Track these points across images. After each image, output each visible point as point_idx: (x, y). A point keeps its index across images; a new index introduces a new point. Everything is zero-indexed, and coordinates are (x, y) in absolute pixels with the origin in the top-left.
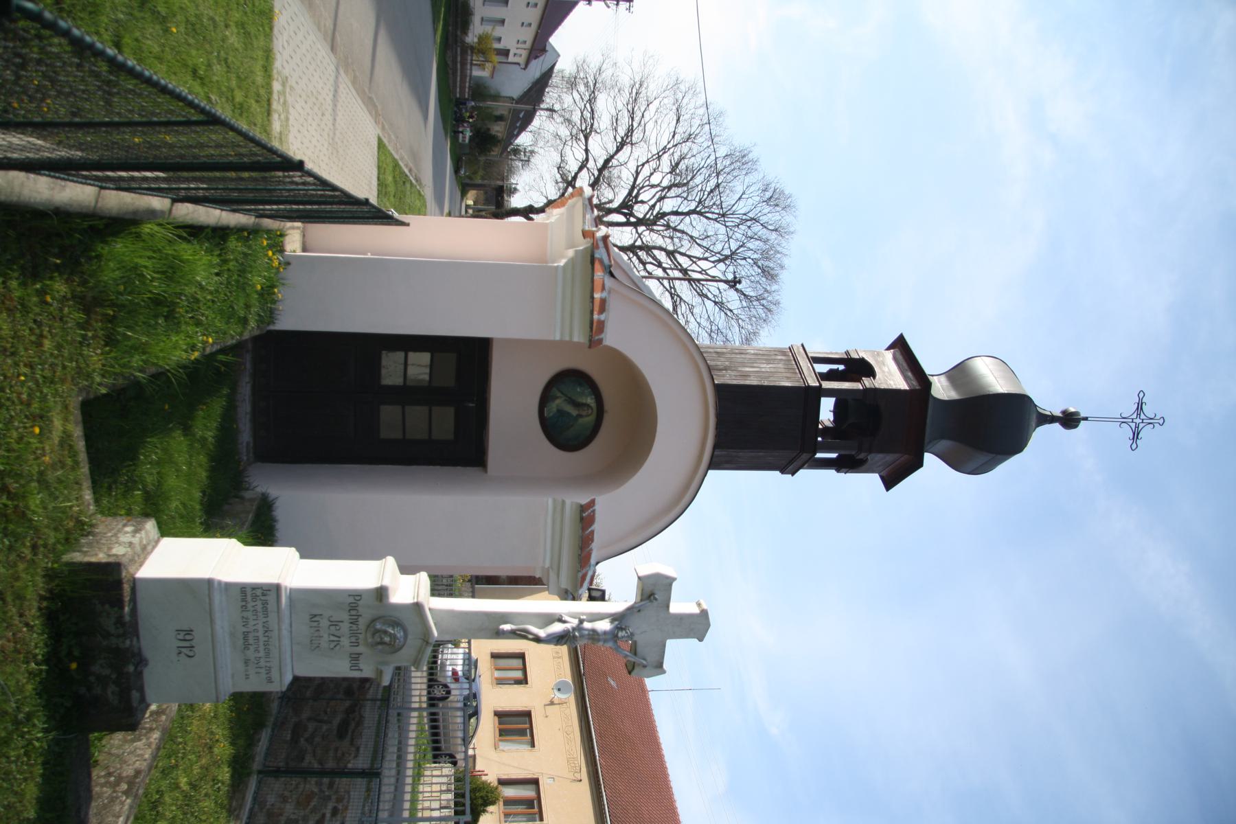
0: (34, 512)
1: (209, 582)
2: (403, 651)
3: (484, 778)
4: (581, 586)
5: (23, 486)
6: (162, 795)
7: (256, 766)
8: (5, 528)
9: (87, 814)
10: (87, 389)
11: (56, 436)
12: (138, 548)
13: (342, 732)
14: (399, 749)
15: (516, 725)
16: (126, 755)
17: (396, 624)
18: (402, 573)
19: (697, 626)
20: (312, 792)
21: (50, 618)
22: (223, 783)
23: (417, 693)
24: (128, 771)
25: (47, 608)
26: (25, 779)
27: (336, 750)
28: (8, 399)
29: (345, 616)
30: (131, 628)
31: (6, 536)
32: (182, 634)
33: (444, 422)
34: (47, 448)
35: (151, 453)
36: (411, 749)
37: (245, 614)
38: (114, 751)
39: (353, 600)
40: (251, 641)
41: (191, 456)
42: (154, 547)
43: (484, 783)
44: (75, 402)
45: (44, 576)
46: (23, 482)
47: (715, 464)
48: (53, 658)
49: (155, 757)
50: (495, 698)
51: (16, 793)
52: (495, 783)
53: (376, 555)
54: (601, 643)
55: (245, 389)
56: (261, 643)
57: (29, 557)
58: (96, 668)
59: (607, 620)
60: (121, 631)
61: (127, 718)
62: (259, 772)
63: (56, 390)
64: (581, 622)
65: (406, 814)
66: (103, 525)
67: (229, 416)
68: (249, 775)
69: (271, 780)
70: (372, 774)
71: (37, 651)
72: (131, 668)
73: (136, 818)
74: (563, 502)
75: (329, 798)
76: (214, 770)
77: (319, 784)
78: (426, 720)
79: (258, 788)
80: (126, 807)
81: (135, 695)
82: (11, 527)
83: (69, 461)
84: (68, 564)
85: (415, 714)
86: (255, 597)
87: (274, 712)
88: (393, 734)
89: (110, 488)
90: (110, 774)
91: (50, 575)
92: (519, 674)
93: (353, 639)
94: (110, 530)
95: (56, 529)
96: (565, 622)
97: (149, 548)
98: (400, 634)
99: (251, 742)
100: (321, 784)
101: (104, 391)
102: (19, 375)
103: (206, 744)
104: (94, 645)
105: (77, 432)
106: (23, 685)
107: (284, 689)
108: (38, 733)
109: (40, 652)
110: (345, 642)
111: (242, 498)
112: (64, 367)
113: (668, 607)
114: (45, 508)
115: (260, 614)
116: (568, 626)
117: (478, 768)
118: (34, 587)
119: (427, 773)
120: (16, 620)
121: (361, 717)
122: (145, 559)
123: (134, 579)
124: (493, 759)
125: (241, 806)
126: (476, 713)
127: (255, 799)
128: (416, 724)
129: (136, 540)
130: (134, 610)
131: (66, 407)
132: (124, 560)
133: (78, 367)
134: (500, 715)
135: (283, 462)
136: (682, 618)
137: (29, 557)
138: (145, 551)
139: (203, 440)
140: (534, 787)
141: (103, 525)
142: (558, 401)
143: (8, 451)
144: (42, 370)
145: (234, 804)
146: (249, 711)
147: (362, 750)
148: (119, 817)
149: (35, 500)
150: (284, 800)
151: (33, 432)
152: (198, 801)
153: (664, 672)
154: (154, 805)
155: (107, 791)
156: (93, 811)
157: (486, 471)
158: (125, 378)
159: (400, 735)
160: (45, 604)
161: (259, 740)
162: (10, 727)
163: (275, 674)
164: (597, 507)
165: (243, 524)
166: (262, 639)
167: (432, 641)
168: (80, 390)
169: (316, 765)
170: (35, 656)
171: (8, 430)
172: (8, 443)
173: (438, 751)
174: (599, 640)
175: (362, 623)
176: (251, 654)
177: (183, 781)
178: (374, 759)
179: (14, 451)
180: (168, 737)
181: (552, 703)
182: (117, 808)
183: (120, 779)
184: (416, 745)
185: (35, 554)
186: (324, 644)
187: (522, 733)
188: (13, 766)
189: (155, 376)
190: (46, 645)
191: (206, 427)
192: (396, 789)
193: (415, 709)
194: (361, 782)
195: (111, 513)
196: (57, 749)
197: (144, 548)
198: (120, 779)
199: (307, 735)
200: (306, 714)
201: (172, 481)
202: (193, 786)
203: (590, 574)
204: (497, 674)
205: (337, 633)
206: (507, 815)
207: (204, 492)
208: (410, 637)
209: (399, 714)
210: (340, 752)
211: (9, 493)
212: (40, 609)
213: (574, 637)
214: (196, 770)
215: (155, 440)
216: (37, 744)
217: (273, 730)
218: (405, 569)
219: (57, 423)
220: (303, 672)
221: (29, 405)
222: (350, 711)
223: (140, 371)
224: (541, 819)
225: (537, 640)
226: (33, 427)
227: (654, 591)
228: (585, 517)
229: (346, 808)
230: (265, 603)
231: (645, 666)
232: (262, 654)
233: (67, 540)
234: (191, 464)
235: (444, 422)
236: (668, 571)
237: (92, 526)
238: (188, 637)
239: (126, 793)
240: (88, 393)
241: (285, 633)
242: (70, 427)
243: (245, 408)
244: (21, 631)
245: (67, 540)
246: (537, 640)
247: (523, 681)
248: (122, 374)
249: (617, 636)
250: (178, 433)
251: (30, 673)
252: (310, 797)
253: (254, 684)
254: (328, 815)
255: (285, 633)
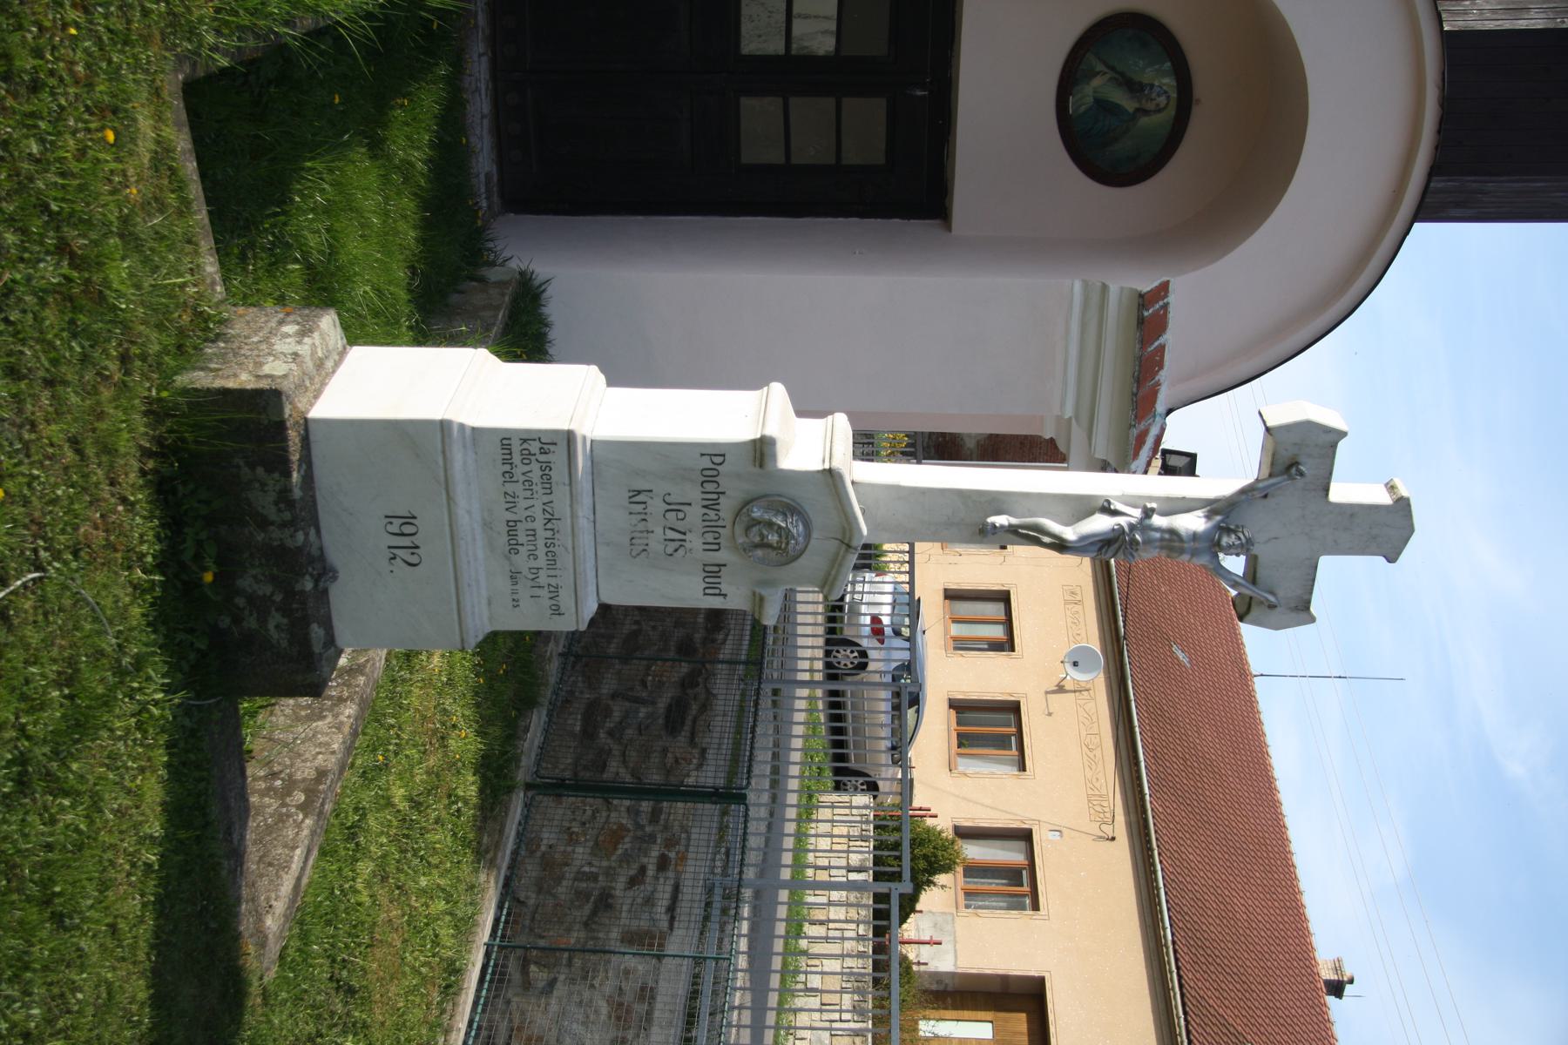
0: (120, 294)
1: (444, 426)
2: (802, 561)
3: (929, 822)
4: (1136, 455)
5: (95, 243)
6: (363, 816)
7: (522, 776)
8: (72, 322)
9: (242, 838)
10: (192, 57)
11: (145, 149)
12: (309, 365)
13: (675, 719)
14: (775, 756)
15: (991, 727)
16: (300, 742)
17: (791, 509)
18: (800, 413)
19: (1385, 530)
20: (622, 827)
21: (163, 489)
22: (466, 803)
23: (805, 665)
24: (305, 771)
25: (155, 471)
26: (142, 770)
27: (665, 751)
28: (52, 73)
29: (694, 494)
30: (304, 512)
31: (74, 336)
32: (397, 522)
33: (864, 130)
34: (131, 172)
35: (314, 190)
36: (796, 756)
37: (510, 488)
38: (277, 735)
39: (710, 462)
40: (522, 538)
41: (387, 199)
42: (337, 364)
43: (928, 830)
44: (172, 82)
45: (146, 414)
46: (94, 236)
47: (1431, 209)
48: (172, 560)
49: (349, 749)
50: (950, 675)
51: (129, 792)
52: (949, 834)
53: (752, 380)
54: (1186, 557)
55: (479, 69)
56: (540, 543)
57: (117, 377)
58: (245, 583)
59: (1200, 513)
60: (287, 516)
61: (304, 673)
62: (529, 787)
63: (135, 57)
64: (1148, 513)
65: (786, 874)
66: (245, 323)
67: (451, 121)
68: (510, 790)
69: (547, 801)
70: (730, 796)
71: (144, 548)
72: (309, 585)
73: (323, 853)
74: (1105, 287)
75: (652, 838)
76: (450, 779)
77: (633, 812)
78: (820, 705)
79: (526, 818)
80: (306, 832)
81: (317, 632)
82: (82, 319)
83: (171, 199)
84: (185, 392)
85: (805, 692)
86: (527, 456)
87: (552, 680)
88: (765, 730)
89: (243, 258)
90: (274, 775)
91: (157, 412)
92: (997, 632)
93: (710, 538)
94: (256, 332)
95: (160, 327)
96: (1115, 513)
97: (329, 364)
98: (797, 529)
99: (513, 734)
100: (637, 813)
101: (224, 62)
102: (65, 26)
103: (435, 731)
104: (239, 540)
105: (182, 142)
106: (126, 607)
107: (583, 627)
108: (154, 688)
109: (149, 550)
110: (695, 542)
111: (482, 280)
112: (146, 13)
113: (1327, 490)
114: (138, 287)
115: (538, 488)
116: (1122, 521)
117: (916, 804)
118: (131, 433)
119: (825, 814)
120: (105, 491)
121: (710, 694)
122: (323, 384)
123: (306, 420)
124: (949, 789)
125: (497, 846)
126: (915, 701)
127: (519, 835)
128: (805, 709)
129: (304, 349)
130: (308, 480)
131: (157, 92)
132: (286, 386)
133: (170, 13)
134: (960, 707)
135: (556, 213)
136: (1353, 513)
137: (117, 377)
138: (322, 370)
139: (406, 168)
140: (1022, 844)
141: (245, 323)
142: (1096, 82)
143: (63, 175)
144: (106, 16)
145: (485, 839)
146: (510, 670)
147: (711, 754)
148: (294, 848)
149: (120, 271)
150: (572, 839)
151: (104, 139)
152: (424, 831)
153: (1312, 620)
154: (352, 833)
155: (272, 804)
156: (250, 836)
157: (948, 226)
158: (257, 36)
159: (777, 730)
160: (151, 464)
161: (527, 730)
162: (111, 679)
163: (566, 599)
164: (1171, 299)
165: (487, 329)
166: (541, 534)
167: (858, 543)
168: (180, 59)
169: (628, 778)
170: (142, 556)
171: (59, 134)
172: (61, 160)
173: (846, 772)
174: (1182, 551)
175: (727, 506)
176: (522, 561)
177: (398, 793)
178: (732, 774)
179: (73, 175)
180: (371, 714)
181: (1060, 689)
182: (291, 833)
183: (290, 785)
184: (805, 750)
185: (127, 373)
186: (656, 543)
187: (1001, 742)
188: (121, 745)
189: (318, 33)
190: (158, 537)
191: (411, 143)
192: (769, 826)
193: (803, 684)
194: (710, 809)
195: (246, 300)
196: (187, 722)
197: (320, 365)
198: (290, 785)
199: (609, 725)
200: (608, 685)
201: (354, 247)
202: (416, 805)
203: (1154, 431)
204: (956, 630)
205: (680, 526)
206: (969, 894)
207: (413, 269)
208: (815, 535)
209: (775, 692)
210: (670, 759)
211: (72, 255)
212: (143, 473)
213: (1134, 542)
214: (420, 776)
215: (319, 165)
216: (156, 712)
217: (549, 715)
218: (806, 408)
219: (145, 123)
220: (619, 596)
221: (90, 86)
222: (688, 683)
223: (287, 24)
224: (1036, 906)
225: (1061, 546)
226: (102, 129)
227: (1299, 457)
228: (1148, 318)
229: (683, 858)
230: (546, 468)
231: (1272, 607)
232: (542, 561)
233: (180, 347)
234: (386, 214)
235: (864, 130)
236: (1330, 418)
237: (222, 322)
238: (408, 529)
239: (303, 807)
240: (194, 65)
241: (584, 523)
242: (168, 132)
243: (480, 107)
244: (115, 512)
245: (180, 347)
246: (1061, 546)
247: (1007, 644)
248: (251, 29)
249: (1218, 544)
250: (359, 154)
251: (135, 587)
252: (617, 836)
253: (528, 617)
254: (651, 871)
255: (584, 523)
